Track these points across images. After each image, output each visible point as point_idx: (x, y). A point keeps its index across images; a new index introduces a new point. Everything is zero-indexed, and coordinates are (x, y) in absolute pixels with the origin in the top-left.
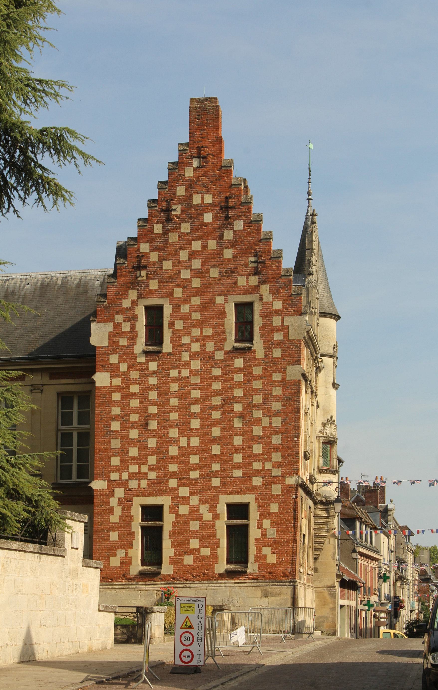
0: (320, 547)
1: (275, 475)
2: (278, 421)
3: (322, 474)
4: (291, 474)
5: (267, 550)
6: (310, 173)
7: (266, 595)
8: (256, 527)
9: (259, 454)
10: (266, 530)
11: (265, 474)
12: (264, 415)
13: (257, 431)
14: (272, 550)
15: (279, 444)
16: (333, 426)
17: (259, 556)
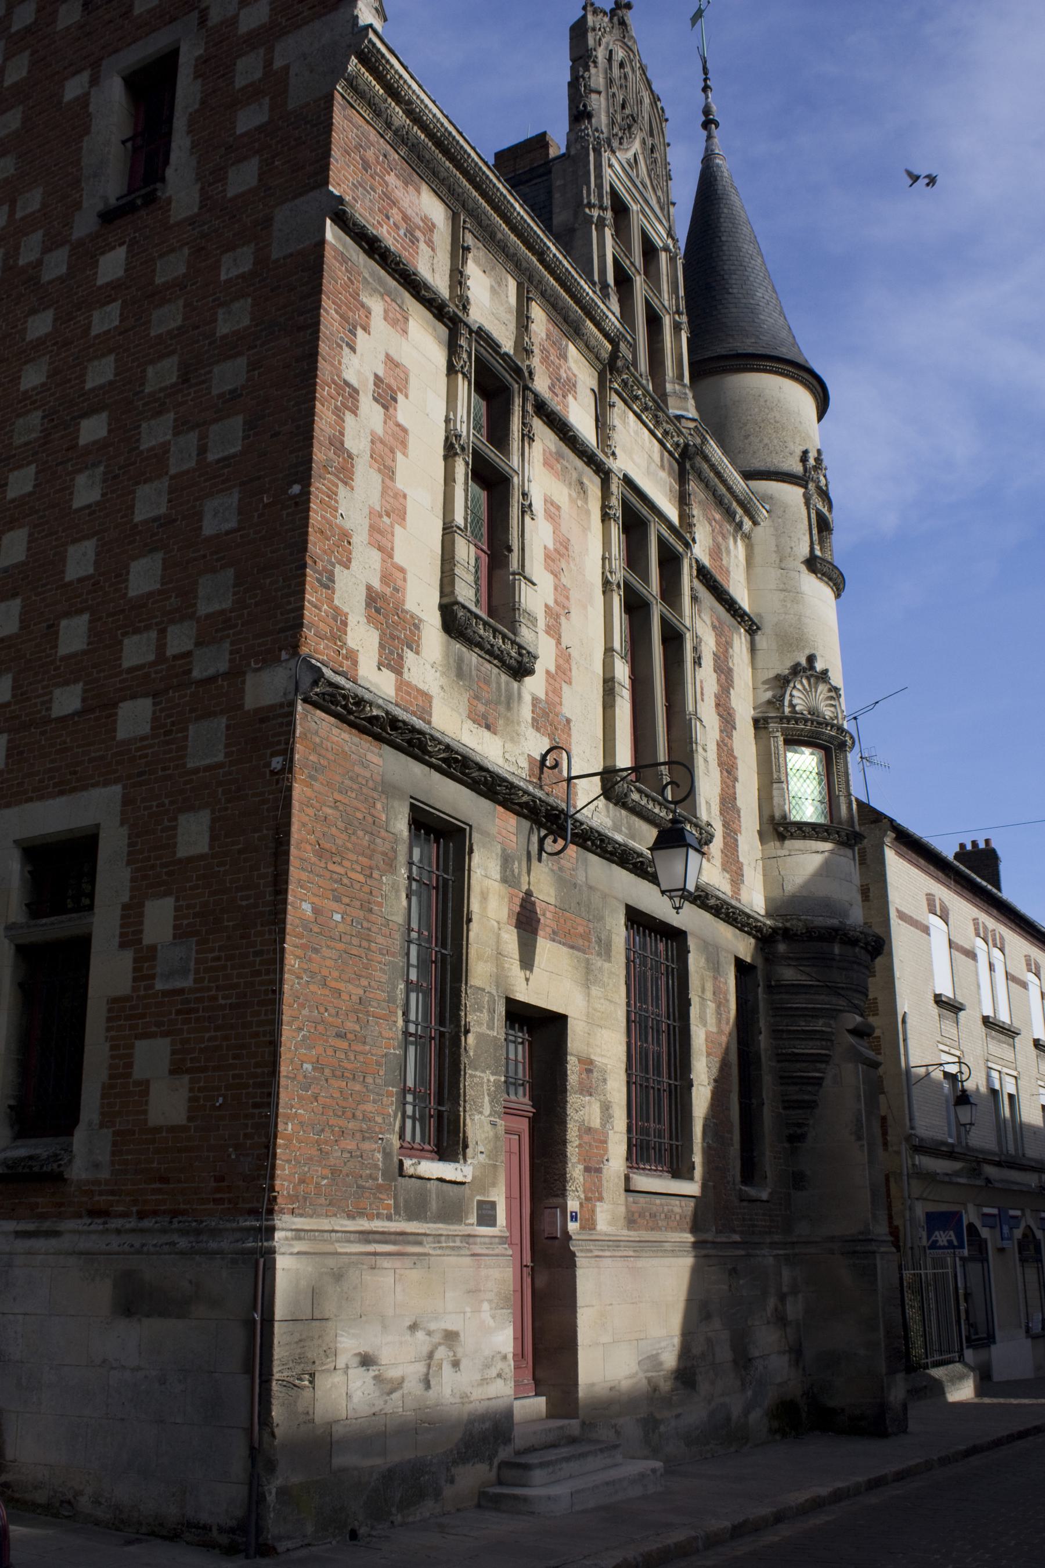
0: (806, 1097)
1: (206, 674)
2: (228, 438)
3: (787, 842)
4: (269, 659)
5: (151, 1057)
6: (705, 71)
7: (134, 1300)
8: (117, 940)
9: (150, 594)
10: (153, 948)
11: (166, 681)
12: (180, 428)
13: (149, 503)
14: (173, 1052)
15: (227, 533)
16: (822, 688)
17: (126, 1092)
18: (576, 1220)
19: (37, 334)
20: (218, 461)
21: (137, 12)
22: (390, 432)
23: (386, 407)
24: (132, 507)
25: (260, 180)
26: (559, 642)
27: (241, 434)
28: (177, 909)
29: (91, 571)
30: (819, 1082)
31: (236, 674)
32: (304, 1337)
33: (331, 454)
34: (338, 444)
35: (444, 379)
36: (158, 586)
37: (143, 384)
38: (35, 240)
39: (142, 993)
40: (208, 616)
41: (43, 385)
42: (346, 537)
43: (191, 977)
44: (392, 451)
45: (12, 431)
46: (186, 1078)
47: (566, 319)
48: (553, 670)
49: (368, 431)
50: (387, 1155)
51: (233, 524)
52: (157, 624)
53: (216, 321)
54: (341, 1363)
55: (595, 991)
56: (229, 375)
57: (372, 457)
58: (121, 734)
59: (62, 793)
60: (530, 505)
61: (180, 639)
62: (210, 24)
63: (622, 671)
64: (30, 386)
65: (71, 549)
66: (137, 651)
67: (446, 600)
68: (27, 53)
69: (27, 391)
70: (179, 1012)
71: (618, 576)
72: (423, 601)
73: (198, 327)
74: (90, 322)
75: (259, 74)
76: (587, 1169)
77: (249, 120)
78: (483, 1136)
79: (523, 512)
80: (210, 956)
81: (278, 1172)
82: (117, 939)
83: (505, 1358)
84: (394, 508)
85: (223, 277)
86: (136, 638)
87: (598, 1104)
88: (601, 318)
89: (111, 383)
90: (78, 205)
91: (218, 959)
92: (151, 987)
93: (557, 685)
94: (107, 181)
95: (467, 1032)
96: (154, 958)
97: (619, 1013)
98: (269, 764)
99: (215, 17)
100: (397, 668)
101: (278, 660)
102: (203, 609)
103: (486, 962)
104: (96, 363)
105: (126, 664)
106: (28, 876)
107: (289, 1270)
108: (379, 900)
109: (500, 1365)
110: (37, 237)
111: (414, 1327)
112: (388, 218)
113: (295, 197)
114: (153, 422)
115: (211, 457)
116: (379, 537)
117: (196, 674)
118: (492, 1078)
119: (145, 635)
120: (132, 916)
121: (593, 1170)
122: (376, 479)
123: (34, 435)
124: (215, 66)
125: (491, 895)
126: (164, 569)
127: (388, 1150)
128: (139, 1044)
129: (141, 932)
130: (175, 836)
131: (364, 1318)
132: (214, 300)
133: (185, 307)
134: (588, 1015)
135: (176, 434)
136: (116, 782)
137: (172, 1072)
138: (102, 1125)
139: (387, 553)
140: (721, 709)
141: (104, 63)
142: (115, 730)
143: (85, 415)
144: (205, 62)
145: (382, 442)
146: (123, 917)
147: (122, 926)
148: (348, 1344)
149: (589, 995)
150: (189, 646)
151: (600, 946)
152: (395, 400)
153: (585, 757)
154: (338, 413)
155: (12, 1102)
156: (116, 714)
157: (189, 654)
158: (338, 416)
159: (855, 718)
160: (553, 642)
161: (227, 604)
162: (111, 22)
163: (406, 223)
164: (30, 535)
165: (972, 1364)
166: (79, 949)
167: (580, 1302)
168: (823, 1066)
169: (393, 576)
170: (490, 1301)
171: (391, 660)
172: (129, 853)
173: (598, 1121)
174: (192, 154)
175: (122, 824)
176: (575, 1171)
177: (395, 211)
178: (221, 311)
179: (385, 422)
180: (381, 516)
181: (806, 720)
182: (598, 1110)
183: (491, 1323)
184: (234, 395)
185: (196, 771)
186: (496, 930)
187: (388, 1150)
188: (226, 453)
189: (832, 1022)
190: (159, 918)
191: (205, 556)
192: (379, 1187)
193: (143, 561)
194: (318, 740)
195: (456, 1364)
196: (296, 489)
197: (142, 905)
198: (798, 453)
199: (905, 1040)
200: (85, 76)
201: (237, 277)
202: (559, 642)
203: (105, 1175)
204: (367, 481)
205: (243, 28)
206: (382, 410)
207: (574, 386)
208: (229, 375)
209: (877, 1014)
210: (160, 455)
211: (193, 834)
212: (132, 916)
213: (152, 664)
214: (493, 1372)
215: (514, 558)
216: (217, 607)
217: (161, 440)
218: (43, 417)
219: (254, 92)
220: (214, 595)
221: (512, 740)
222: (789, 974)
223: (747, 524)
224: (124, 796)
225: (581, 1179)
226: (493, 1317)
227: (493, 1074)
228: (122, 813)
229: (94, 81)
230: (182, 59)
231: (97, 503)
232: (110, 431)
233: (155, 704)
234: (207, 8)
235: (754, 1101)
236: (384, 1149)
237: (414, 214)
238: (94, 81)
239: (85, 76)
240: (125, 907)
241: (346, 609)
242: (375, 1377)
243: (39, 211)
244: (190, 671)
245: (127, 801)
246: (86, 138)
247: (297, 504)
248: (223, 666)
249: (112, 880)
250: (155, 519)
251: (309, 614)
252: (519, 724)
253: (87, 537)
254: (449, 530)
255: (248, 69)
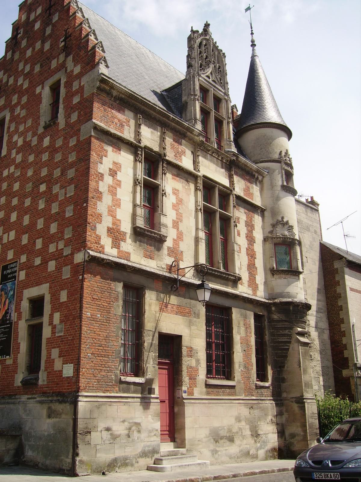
2: (71, 191)
6: (251, 28)
9: (55, 233)
10: (55, 325)
11: (58, 256)
15: (71, 216)
18: (186, 393)
19: (31, 161)
20: (69, 197)
21: (52, 68)
22: (115, 183)
23: (113, 177)
24: (51, 209)
25: (78, 118)
26: (178, 230)
27: (73, 190)
28: (60, 315)
29: (43, 227)
30: (288, 349)
31: (72, 254)
32: (87, 422)
33: (95, 194)
34: (97, 190)
35: (132, 163)
36: (56, 231)
37: (53, 175)
38: (30, 134)
39: (53, 337)
40: (67, 239)
41: (32, 175)
42: (100, 215)
43: (63, 332)
44: (116, 188)
45: (26, 188)
46: (62, 358)
47: (180, 134)
48: (175, 238)
49: (107, 185)
50: (116, 376)
51: (72, 214)
52: (56, 241)
53: (68, 158)
54: (99, 429)
55: (193, 327)
56: (71, 173)
57: (108, 191)
58: (49, 270)
59: (37, 285)
60: (165, 193)
61: (61, 245)
62: (68, 72)
63: (202, 235)
64: (30, 175)
65: (38, 220)
66: (52, 248)
67: (134, 226)
68: (28, 80)
69: (29, 177)
70: (61, 341)
71: (201, 206)
72: (126, 227)
73: (65, 159)
74: (42, 158)
75: (78, 87)
76: (190, 379)
77: (76, 100)
78: (150, 370)
79: (162, 196)
80: (67, 327)
81: (80, 381)
82: (48, 323)
83: (157, 430)
84: (117, 203)
85: (70, 146)
86: (52, 244)
87: (195, 360)
88: (192, 131)
89: (47, 175)
90: (39, 124)
91: (68, 328)
92: (55, 335)
93: (177, 242)
94: (44, 117)
95: (144, 342)
96: (55, 328)
97: (203, 333)
98: (79, 278)
99: (68, 71)
100: (118, 247)
101: (81, 250)
102: (66, 237)
103: (151, 323)
104: (43, 169)
105: (50, 252)
106: (31, 307)
107: (82, 406)
108: (113, 310)
109: (155, 432)
110: (30, 133)
111: (124, 421)
112: (113, 123)
113: (85, 123)
114: (55, 186)
115: (68, 196)
116: (111, 213)
117: (64, 254)
118: (153, 355)
119: (54, 244)
120: (51, 316)
121: (193, 378)
122: (110, 197)
123: (30, 189)
124: (68, 84)
125: (153, 304)
126: (58, 226)
127: (116, 375)
128: (52, 350)
129: (53, 321)
130: (60, 296)
131: (107, 418)
132: (68, 152)
133: (62, 154)
134: (190, 335)
135: (60, 189)
136: (48, 282)
137: (59, 357)
138: (45, 371)
139: (114, 217)
140: (248, 238)
141: (45, 82)
142: (47, 269)
143: (41, 184)
144: (66, 83)
145: (112, 187)
146: (49, 317)
147: (49, 320)
148: (102, 425)
149: (190, 329)
150: (63, 247)
151: (195, 315)
152: (116, 174)
153: (187, 262)
154: (97, 182)
155: (28, 365)
156: (48, 265)
157: (63, 249)
158: (97, 183)
159: (342, 222)
160: (176, 230)
161: (71, 236)
162: (46, 71)
163: (119, 122)
164: (30, 217)
165: (342, 438)
166: (41, 325)
167: (186, 416)
168: (289, 344)
169: (116, 222)
170: (151, 415)
171: (116, 244)
172: (51, 301)
173: (195, 364)
174: (63, 110)
175: (49, 294)
176: (186, 379)
177: (115, 120)
178: (70, 155)
179: (113, 181)
180: (111, 207)
181: (280, 237)
182: (195, 362)
183: (152, 421)
184: (72, 179)
185: (64, 279)
186: (155, 314)
187: (116, 375)
188: (70, 195)
189: (291, 331)
190: (57, 316)
191: (66, 223)
192: (113, 385)
193: (53, 224)
194: (91, 270)
195: (139, 432)
196: (85, 205)
197: (53, 314)
198: (278, 152)
199: (353, 332)
200: (40, 87)
201: (73, 145)
202: (178, 230)
203: (45, 383)
204: (107, 199)
205: (75, 73)
206: (112, 178)
207: (185, 152)
208: (71, 173)
209: (344, 323)
210: (57, 195)
211: (64, 296)
212: (51, 316)
213: (55, 251)
214: (153, 434)
215: (160, 209)
216: (69, 237)
217: (57, 191)
218: (32, 184)
219: (77, 92)
220: (68, 234)
221: (160, 261)
222: (275, 317)
223: (260, 178)
224: (50, 286)
225: (188, 381)
226: (153, 419)
227: (153, 353)
228: (49, 290)
229: (43, 88)
230: (62, 82)
231: (44, 208)
232: (46, 188)
233: (56, 262)
234: (67, 67)
235: (265, 356)
236: (115, 375)
237: (122, 119)
238: (43, 88)
239: (40, 87)
240: (50, 315)
241: (100, 234)
242: (111, 434)
243: (31, 125)
244: (63, 253)
245: (50, 288)
246: (41, 105)
247: (85, 209)
248: (70, 252)
249: (47, 308)
250: (56, 213)
251: (88, 238)
252: (162, 256)
253: (41, 217)
254: (135, 206)
255: (75, 86)
